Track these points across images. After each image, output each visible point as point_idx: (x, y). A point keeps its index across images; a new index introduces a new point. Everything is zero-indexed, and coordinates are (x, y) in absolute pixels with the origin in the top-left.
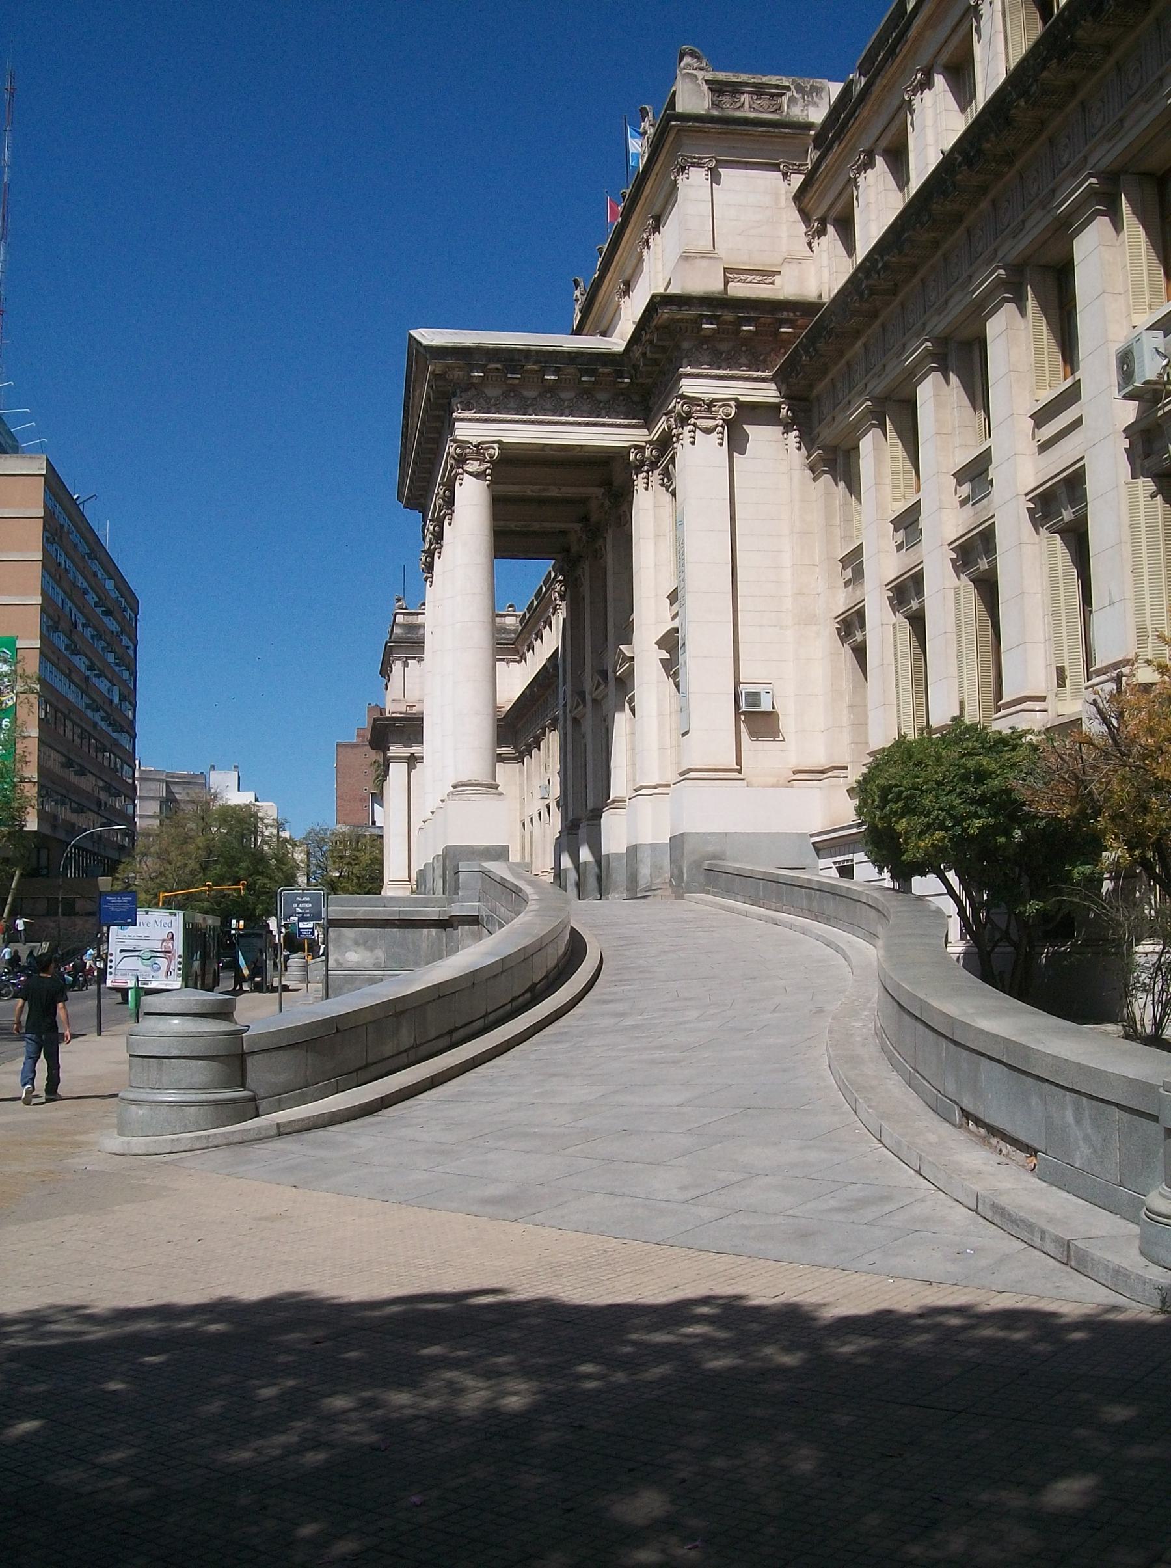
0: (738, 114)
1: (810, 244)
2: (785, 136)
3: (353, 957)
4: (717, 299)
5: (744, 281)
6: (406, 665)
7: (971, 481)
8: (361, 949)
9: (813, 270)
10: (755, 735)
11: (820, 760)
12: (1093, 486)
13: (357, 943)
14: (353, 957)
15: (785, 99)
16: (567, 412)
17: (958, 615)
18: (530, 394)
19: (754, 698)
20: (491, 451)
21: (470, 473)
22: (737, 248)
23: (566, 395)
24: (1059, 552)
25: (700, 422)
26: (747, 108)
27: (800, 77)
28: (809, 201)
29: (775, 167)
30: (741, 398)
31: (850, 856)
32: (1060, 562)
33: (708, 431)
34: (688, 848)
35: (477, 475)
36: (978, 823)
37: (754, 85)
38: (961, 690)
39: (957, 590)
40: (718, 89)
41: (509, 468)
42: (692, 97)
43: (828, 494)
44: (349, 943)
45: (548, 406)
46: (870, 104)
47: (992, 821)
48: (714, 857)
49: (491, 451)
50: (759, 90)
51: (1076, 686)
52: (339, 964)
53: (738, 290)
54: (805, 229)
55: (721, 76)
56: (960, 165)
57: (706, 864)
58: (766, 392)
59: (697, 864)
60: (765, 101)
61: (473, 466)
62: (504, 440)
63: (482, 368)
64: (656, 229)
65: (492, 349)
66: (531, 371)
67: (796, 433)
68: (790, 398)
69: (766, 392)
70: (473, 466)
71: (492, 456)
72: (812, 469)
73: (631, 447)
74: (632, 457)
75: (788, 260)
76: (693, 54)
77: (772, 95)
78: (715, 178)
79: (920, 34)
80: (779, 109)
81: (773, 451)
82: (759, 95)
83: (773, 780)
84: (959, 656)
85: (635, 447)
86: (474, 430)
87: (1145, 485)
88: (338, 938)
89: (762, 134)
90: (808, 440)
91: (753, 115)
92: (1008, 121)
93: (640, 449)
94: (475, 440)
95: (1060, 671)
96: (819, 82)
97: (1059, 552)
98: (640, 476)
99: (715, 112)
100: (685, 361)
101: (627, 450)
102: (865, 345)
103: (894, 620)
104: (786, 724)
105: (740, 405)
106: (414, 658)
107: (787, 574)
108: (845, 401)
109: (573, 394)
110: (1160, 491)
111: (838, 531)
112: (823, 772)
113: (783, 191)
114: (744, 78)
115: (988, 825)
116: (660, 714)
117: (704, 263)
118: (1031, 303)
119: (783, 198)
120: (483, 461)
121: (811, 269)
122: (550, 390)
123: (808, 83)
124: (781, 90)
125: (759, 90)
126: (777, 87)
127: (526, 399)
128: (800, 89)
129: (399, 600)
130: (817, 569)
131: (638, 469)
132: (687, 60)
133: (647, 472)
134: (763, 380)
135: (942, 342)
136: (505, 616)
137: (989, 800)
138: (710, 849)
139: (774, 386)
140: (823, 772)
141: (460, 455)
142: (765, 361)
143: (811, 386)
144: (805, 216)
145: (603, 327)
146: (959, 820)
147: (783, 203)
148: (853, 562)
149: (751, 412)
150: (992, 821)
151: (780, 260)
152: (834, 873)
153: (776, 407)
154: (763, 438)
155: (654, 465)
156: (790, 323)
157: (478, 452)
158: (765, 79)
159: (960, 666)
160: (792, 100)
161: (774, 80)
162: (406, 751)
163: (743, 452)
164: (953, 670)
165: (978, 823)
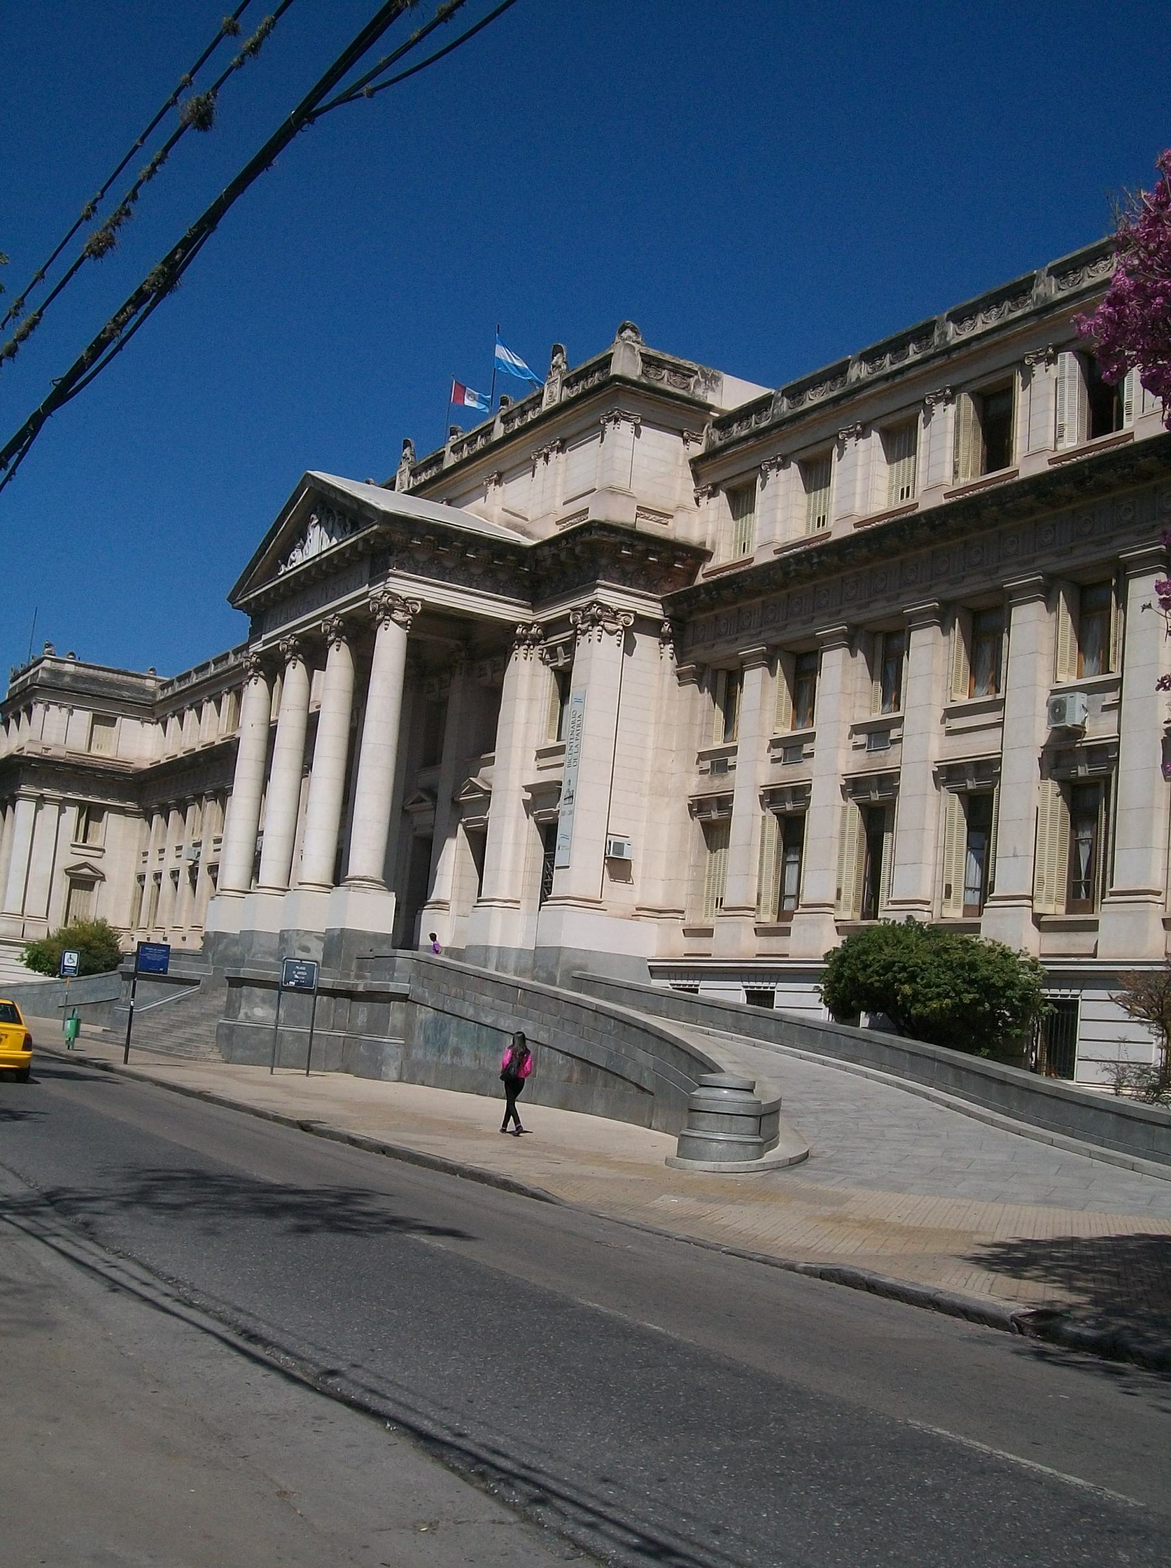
1: (697, 500)
2: (693, 411)
3: (259, 1012)
4: (627, 531)
5: (647, 518)
6: (47, 708)
7: (869, 734)
8: (266, 1007)
9: (697, 520)
10: (614, 876)
11: (658, 901)
12: (1008, 773)
13: (264, 1001)
14: (259, 1012)
15: (692, 381)
16: (474, 584)
17: (843, 824)
18: (449, 564)
19: (619, 847)
20: (414, 606)
21: (396, 622)
22: (650, 493)
24: (956, 808)
26: (666, 382)
27: (705, 364)
28: (703, 469)
30: (639, 612)
31: (697, 982)
32: (956, 815)
34: (563, 958)
36: (971, 996)
37: (673, 364)
38: (840, 879)
39: (844, 809)
40: (648, 360)
42: (626, 363)
43: (694, 699)
44: (257, 1000)
45: (461, 577)
46: (798, 424)
47: (977, 996)
49: (414, 606)
50: (676, 369)
51: (957, 899)
52: (248, 1017)
53: (647, 526)
54: (694, 487)
55: (652, 352)
56: (923, 525)
57: (576, 973)
58: (653, 610)
60: (678, 379)
61: (399, 616)
62: (426, 599)
65: (434, 525)
66: (456, 547)
67: (671, 646)
68: (674, 619)
69: (653, 610)
70: (399, 616)
71: (414, 611)
73: (519, 623)
74: (519, 631)
75: (680, 508)
76: (633, 329)
77: (684, 375)
78: (638, 433)
79: (865, 399)
80: (687, 388)
81: (653, 658)
82: (676, 373)
84: (841, 857)
85: (523, 623)
86: (410, 587)
87: (1052, 786)
89: (676, 406)
90: (680, 654)
91: (669, 388)
93: (528, 627)
94: (404, 595)
96: (717, 373)
97: (956, 808)
98: (522, 648)
100: (601, 575)
101: (514, 625)
102: (763, 602)
104: (636, 871)
105: (639, 618)
106: (56, 704)
107: (650, 754)
108: (733, 636)
111: (697, 730)
112: (660, 912)
113: (682, 452)
114: (667, 357)
115: (974, 998)
117: (624, 499)
118: (956, 632)
120: (407, 612)
121: (697, 520)
122: (465, 564)
123: (710, 372)
124: (688, 373)
125: (676, 369)
126: (689, 369)
127: (445, 568)
128: (704, 375)
129: (49, 645)
130: (673, 754)
131: (521, 640)
132: (628, 333)
133: (529, 645)
134: (654, 600)
135: (855, 628)
136: (145, 678)
137: (977, 982)
138: (578, 961)
139: (660, 606)
140: (660, 912)
141: (390, 605)
142: (656, 586)
144: (697, 477)
146: (958, 993)
147: (681, 462)
150: (977, 996)
152: (742, 998)
153: (660, 623)
154: (645, 643)
155: (536, 641)
157: (404, 605)
158: (682, 362)
159: (841, 864)
161: (687, 363)
163: (630, 655)
164: (834, 864)
165: (971, 996)
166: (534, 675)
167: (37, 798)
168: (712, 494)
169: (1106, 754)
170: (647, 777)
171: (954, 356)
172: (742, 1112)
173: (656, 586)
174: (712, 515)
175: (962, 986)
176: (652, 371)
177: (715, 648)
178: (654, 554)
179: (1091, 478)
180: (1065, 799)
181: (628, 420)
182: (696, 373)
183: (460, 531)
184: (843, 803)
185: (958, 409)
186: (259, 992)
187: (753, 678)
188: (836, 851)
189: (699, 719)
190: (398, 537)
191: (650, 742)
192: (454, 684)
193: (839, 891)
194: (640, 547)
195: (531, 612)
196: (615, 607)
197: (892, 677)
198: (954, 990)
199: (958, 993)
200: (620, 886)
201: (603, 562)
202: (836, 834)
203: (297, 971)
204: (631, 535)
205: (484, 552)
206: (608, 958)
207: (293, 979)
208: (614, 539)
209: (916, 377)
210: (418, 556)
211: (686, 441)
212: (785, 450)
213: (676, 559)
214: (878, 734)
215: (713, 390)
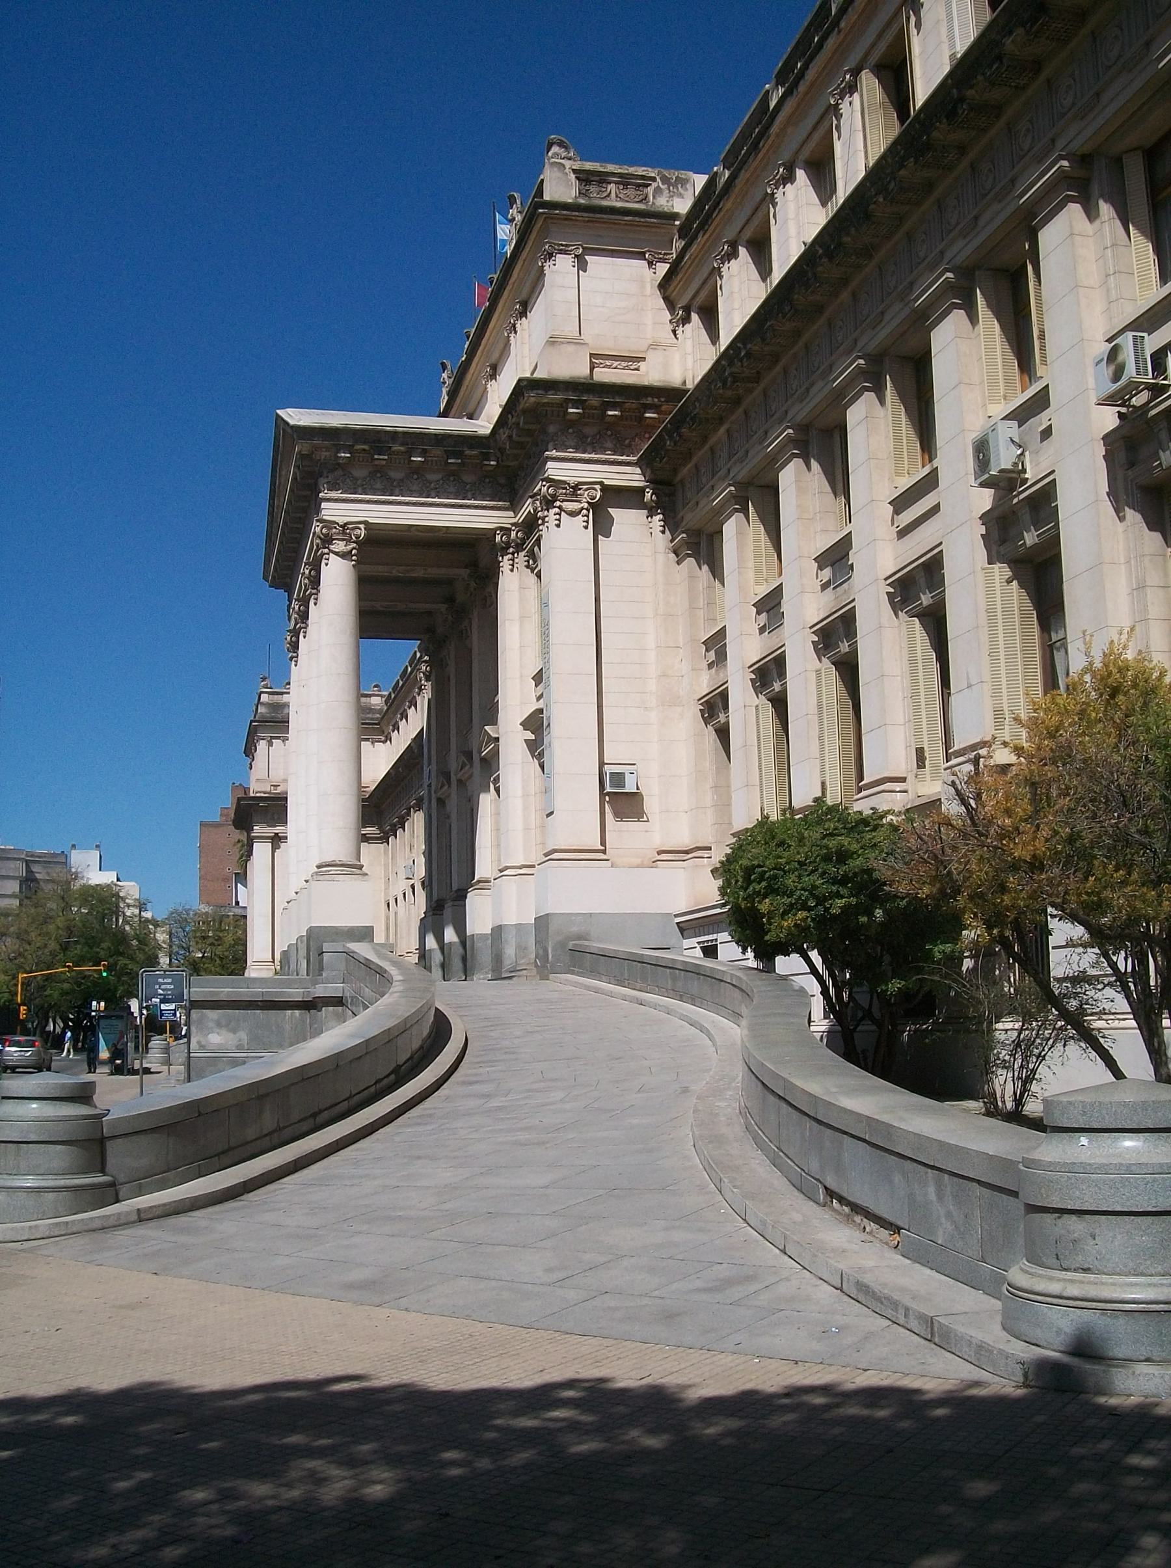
0: (605, 203)
1: (674, 332)
5: (609, 367)
6: (270, 744)
8: (224, 1032)
9: (677, 357)
10: (619, 815)
11: (684, 840)
13: (219, 1024)
15: (650, 190)
17: (819, 696)
19: (618, 779)
21: (336, 554)
22: (603, 334)
23: (432, 477)
25: (565, 505)
26: (614, 197)
29: (641, 256)
30: (607, 482)
31: (714, 936)
33: (573, 514)
34: (552, 928)
35: (344, 555)
37: (621, 175)
38: (823, 771)
39: (818, 671)
40: (584, 178)
41: (375, 549)
42: (560, 186)
43: (692, 577)
44: (211, 1024)
47: (853, 900)
50: (625, 181)
51: (935, 766)
52: (202, 1046)
53: (604, 375)
55: (589, 166)
56: (820, 257)
57: (570, 945)
58: (631, 476)
59: (562, 944)
60: (631, 191)
61: (339, 546)
63: (349, 449)
64: (523, 314)
66: (398, 453)
67: (661, 516)
68: (656, 482)
69: (631, 476)
70: (339, 546)
71: (358, 537)
72: (676, 553)
73: (497, 529)
74: (498, 538)
75: (655, 346)
76: (561, 144)
77: (639, 185)
78: (582, 265)
79: (783, 129)
81: (638, 534)
82: (626, 185)
83: (639, 861)
84: (821, 738)
85: (501, 529)
86: (340, 510)
87: (1001, 571)
88: (200, 1021)
90: (671, 524)
91: (619, 204)
92: (868, 216)
93: (506, 531)
96: (684, 174)
97: (918, 638)
98: (506, 558)
100: (550, 446)
101: (493, 532)
102: (728, 431)
103: (757, 702)
104: (651, 805)
105: (605, 489)
106: (278, 738)
107: (652, 656)
110: (1015, 576)
112: (687, 852)
114: (611, 168)
116: (525, 795)
117: (570, 348)
119: (648, 286)
120: (349, 541)
121: (676, 357)
122: (417, 472)
123: (673, 175)
125: (625, 181)
126: (643, 177)
128: (665, 180)
129: (264, 679)
131: (504, 550)
133: (513, 554)
134: (628, 464)
136: (370, 696)
138: (574, 929)
139: (638, 470)
140: (687, 852)
141: (326, 535)
142: (629, 446)
143: (675, 471)
144: (670, 304)
145: (470, 408)
146: (821, 900)
147: (648, 290)
148: (717, 644)
149: (616, 496)
150: (853, 900)
151: (644, 348)
152: (698, 953)
153: (641, 491)
154: (625, 519)
155: (519, 547)
157: (344, 533)
158: (632, 170)
159: (822, 749)
160: (658, 191)
161: (640, 171)
162: (270, 831)
165: (840, 902)
166: (522, 588)
167: (272, 838)
168: (686, 320)
169: (1044, 502)
170: (652, 686)
171: (843, 24)
172: (33, 1138)
176: (593, 189)
177: (701, 505)
178: (613, 406)
179: (962, 100)
180: (1022, 585)
181: (565, 252)
182: (654, 179)
183: (396, 432)
185: (861, 96)
188: (816, 733)
189: (701, 603)
191: (651, 641)
195: (511, 514)
196: (572, 481)
197: (839, 477)
202: (813, 709)
203: (160, 984)
204: (581, 388)
205: (437, 451)
206: (618, 921)
207: (156, 995)
208: (553, 397)
210: (394, 474)
213: (647, 408)
214: (837, 559)
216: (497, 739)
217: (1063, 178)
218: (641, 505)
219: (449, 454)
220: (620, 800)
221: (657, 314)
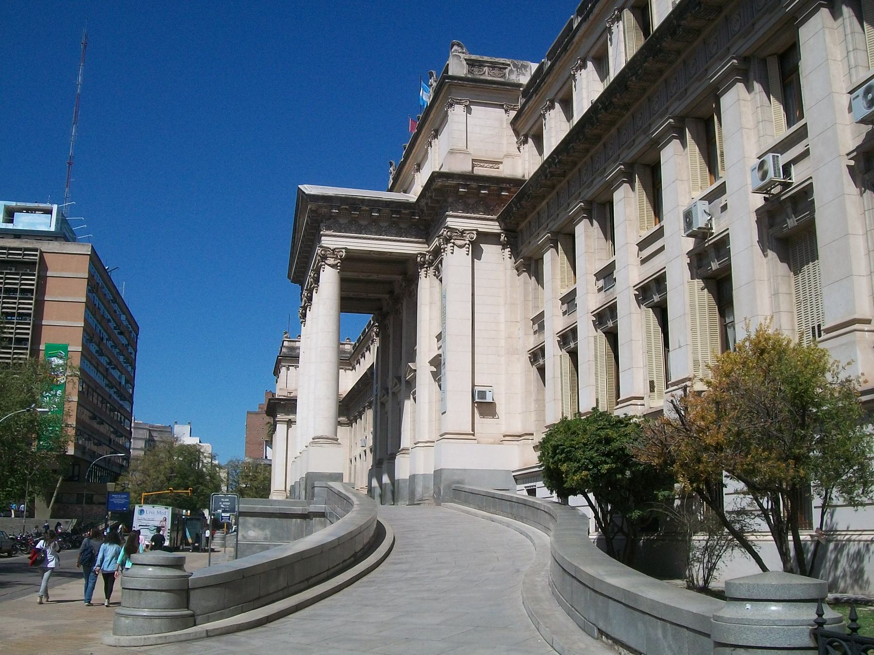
0: (482, 77)
1: (519, 148)
2: (508, 90)
3: (252, 534)
9: (520, 162)
10: (483, 414)
11: (519, 430)
13: (254, 525)
14: (252, 534)
15: (507, 71)
17: (596, 350)
18: (363, 223)
19: (482, 394)
21: (329, 265)
22: (481, 148)
26: (487, 74)
29: (501, 106)
31: (534, 484)
33: (461, 247)
34: (443, 477)
35: (332, 266)
36: (606, 467)
38: (597, 393)
39: (595, 337)
40: (471, 63)
41: (350, 262)
42: (457, 67)
43: (525, 283)
44: (250, 525)
47: (614, 466)
48: (458, 482)
50: (493, 66)
51: (660, 391)
52: (244, 537)
53: (480, 171)
55: (473, 57)
57: (454, 486)
58: (493, 227)
59: (449, 486)
60: (496, 71)
61: (331, 261)
64: (436, 136)
68: (506, 230)
69: (493, 227)
70: (331, 261)
74: (419, 259)
75: (507, 156)
76: (459, 45)
77: (501, 68)
78: (469, 111)
80: (504, 76)
81: (497, 260)
82: (494, 68)
83: (492, 440)
84: (596, 374)
85: (421, 254)
87: (698, 283)
90: (515, 254)
91: (490, 78)
94: (332, 247)
95: (652, 384)
96: (525, 63)
99: (470, 76)
100: (449, 209)
101: (416, 256)
104: (500, 409)
105: (479, 233)
107: (502, 326)
109: (386, 224)
110: (706, 286)
112: (520, 436)
114: (486, 58)
117: (462, 156)
119: (505, 123)
120: (336, 258)
123: (520, 63)
124: (503, 67)
125: (493, 66)
126: (503, 64)
128: (515, 66)
129: (286, 333)
132: (455, 47)
134: (492, 220)
137: (613, 454)
138: (456, 478)
139: (497, 224)
140: (520, 436)
142: (493, 210)
144: (517, 133)
145: (405, 187)
146: (596, 465)
149: (485, 237)
150: (614, 466)
153: (498, 235)
154: (490, 251)
155: (430, 264)
156: (507, 190)
158: (497, 60)
159: (597, 380)
160: (511, 71)
161: (502, 60)
164: (593, 382)
165: (606, 467)
169: (722, 246)
170: (502, 343)
172: (149, 587)
173: (493, 210)
174: (527, 155)
175: (598, 459)
178: (484, 188)
179: (679, 26)
180: (709, 291)
182: (509, 65)
184: (595, 333)
186: (251, 520)
187: (548, 257)
190: (324, 210)
192: (383, 300)
193: (597, 400)
194: (474, 185)
198: (591, 462)
199: (596, 465)
200: (489, 421)
201: (450, 200)
202: (592, 358)
204: (467, 178)
205: (386, 210)
209: (601, 10)
211: (506, 111)
212: (551, 97)
213: (503, 189)
214: (607, 275)
215: (524, 74)
216: (415, 370)
217: (734, 70)
218: (498, 243)
219: (393, 212)
220: (484, 407)
221: (509, 138)
